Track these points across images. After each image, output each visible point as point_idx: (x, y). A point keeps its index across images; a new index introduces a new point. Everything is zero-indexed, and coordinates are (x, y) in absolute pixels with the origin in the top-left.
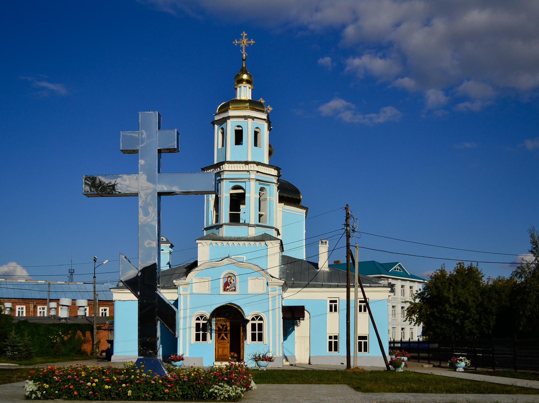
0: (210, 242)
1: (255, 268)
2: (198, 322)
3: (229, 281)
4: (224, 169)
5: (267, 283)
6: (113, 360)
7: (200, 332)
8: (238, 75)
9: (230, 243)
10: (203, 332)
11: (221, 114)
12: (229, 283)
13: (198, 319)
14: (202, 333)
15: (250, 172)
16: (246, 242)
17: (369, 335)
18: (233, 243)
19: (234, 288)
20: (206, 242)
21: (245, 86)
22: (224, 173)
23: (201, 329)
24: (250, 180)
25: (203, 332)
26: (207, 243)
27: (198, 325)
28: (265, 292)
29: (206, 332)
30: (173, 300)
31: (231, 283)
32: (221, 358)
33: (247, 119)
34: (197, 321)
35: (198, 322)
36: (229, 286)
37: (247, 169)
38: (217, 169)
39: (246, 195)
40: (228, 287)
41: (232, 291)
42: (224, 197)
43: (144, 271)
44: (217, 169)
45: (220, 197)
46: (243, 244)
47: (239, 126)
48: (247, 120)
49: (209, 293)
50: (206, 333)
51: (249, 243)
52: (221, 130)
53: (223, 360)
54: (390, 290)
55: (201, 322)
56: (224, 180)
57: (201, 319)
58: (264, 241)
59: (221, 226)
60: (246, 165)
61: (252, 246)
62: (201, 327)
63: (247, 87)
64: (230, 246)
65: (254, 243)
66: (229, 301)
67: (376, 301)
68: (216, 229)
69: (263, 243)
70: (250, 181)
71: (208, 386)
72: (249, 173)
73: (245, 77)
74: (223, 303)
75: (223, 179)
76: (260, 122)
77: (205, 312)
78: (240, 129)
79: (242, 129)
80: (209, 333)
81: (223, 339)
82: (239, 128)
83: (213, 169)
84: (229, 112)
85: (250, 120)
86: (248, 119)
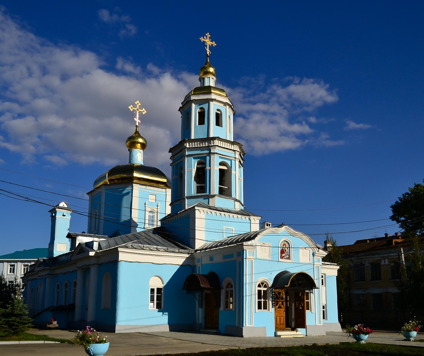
1: (304, 238)
2: (260, 289)
3: (284, 249)
4: (215, 144)
5: (313, 254)
6: (118, 330)
7: (261, 299)
8: (205, 68)
9: (223, 213)
10: (264, 300)
11: (200, 95)
12: (284, 251)
13: (259, 286)
14: (263, 301)
15: (236, 152)
17: (326, 305)
19: (288, 256)
20: (203, 209)
21: (213, 78)
22: (216, 147)
23: (262, 297)
25: (264, 300)
26: (200, 210)
27: (259, 292)
28: (312, 262)
29: (267, 300)
30: (178, 265)
31: (285, 250)
32: (279, 327)
34: (258, 288)
35: (260, 289)
36: (284, 254)
38: (204, 143)
40: (283, 255)
41: (286, 259)
43: (393, 220)
44: (204, 143)
45: (210, 170)
46: (228, 215)
47: (218, 110)
48: (225, 107)
49: (269, 259)
50: (267, 301)
51: (237, 216)
52: (199, 109)
53: (281, 329)
54: (339, 268)
55: (263, 289)
56: (216, 155)
57: (262, 286)
58: (249, 215)
59: (214, 196)
60: (232, 145)
61: (239, 219)
62: (262, 295)
65: (241, 217)
66: (285, 268)
67: (330, 277)
68: (204, 199)
69: (247, 218)
70: (235, 161)
71: (90, 350)
72: (235, 154)
73: (211, 70)
74: (283, 269)
75: (214, 153)
77: (266, 279)
78: (219, 112)
79: (220, 113)
80: (270, 301)
81: (280, 307)
82: (218, 111)
83: (198, 143)
84: (211, 95)
85: (228, 107)
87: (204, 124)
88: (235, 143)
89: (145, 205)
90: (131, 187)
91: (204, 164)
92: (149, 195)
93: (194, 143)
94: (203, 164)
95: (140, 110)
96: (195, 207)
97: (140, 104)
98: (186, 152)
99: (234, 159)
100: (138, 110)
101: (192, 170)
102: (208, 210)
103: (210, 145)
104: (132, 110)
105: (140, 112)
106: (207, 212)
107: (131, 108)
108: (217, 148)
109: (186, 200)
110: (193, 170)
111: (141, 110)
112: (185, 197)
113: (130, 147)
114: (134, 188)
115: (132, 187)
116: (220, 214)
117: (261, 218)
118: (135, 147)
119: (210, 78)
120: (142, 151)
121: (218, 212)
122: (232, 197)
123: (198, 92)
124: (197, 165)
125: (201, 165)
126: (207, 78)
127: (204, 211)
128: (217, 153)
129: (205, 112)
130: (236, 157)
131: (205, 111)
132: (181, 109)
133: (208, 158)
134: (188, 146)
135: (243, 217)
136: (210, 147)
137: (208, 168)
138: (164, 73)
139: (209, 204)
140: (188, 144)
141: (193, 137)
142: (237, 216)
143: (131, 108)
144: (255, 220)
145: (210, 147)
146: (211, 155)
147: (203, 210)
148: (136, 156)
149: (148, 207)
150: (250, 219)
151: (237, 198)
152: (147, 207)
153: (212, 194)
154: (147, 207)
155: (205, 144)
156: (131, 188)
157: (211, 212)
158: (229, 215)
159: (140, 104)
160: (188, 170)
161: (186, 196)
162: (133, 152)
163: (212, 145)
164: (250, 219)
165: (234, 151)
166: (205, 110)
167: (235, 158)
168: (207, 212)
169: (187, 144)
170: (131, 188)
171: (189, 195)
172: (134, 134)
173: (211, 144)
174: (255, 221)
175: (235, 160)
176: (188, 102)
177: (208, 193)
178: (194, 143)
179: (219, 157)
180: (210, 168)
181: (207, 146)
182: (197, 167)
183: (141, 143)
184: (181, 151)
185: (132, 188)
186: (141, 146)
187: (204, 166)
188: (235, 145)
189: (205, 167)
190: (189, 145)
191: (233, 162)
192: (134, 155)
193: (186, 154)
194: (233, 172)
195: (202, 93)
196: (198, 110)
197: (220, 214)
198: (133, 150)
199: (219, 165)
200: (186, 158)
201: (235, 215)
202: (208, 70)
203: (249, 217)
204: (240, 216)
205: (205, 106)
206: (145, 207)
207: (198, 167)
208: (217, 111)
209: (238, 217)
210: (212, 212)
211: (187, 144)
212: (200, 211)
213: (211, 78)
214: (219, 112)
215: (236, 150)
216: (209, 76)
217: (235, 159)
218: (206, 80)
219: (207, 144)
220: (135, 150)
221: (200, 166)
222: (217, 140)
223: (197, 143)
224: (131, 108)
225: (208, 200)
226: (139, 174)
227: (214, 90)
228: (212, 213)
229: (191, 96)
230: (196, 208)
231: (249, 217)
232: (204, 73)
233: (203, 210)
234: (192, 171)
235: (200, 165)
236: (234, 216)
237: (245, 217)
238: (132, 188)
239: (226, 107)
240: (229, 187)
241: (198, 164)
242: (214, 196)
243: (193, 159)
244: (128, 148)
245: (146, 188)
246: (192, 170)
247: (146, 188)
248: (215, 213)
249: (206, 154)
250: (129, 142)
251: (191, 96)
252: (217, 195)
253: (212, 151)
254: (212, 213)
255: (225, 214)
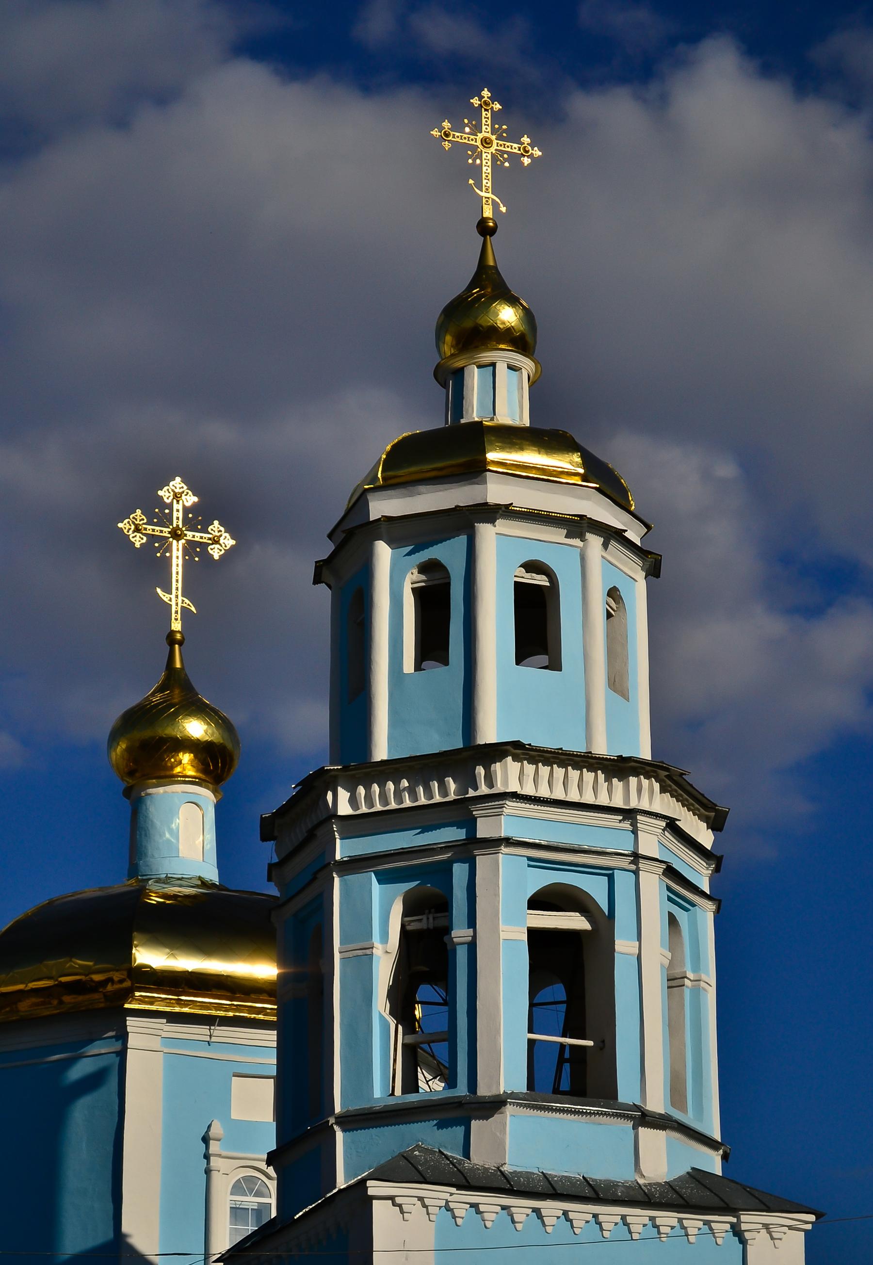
0: (447, 1196)
4: (499, 788)
9: (552, 1208)
11: (422, 488)
16: (638, 1211)
18: (595, 1216)
21: (517, 364)
24: (643, 865)
26: (398, 1200)
33: (583, 539)
37: (618, 802)
38: (435, 785)
39: (617, 947)
42: (501, 941)
44: (435, 785)
45: (472, 947)
47: (532, 566)
48: (577, 542)
51: (652, 1219)
52: (415, 571)
56: (504, 849)
59: (495, 1105)
60: (615, 780)
63: (523, 370)
64: (519, 1227)
65: (674, 1222)
68: (441, 1126)
69: (722, 1223)
70: (636, 873)
72: (635, 832)
75: (495, 843)
76: (619, 560)
78: (541, 580)
79: (548, 584)
83: (405, 783)
84: (486, 483)
85: (595, 541)
86: (588, 536)
87: (444, 660)
88: (633, 764)
89: (207, 1148)
90: (116, 1038)
91: (443, 905)
92: (233, 1078)
93: (382, 786)
94: (436, 912)
95: (190, 535)
96: (369, 1183)
97: (190, 499)
98: (338, 841)
99: (625, 863)
100: (176, 535)
101: (368, 952)
102: (451, 1194)
103: (471, 793)
104: (138, 541)
105: (191, 548)
106: (448, 1209)
107: (137, 530)
108: (512, 805)
109: (340, 1135)
110: (378, 950)
111: (198, 536)
112: (332, 1120)
113: (131, 773)
114: (132, 1041)
115: (123, 1036)
116: (537, 1211)
117: (812, 1218)
118: (163, 774)
119: (493, 365)
120: (207, 796)
121: (522, 1206)
122: (616, 1098)
123: (413, 469)
124: (405, 914)
125: (424, 917)
126: (479, 367)
127: (427, 1201)
128: (508, 842)
129: (448, 585)
130: (642, 851)
131: (449, 584)
132: (326, 573)
133: (459, 871)
134: (344, 809)
135: (694, 1223)
136: (472, 808)
137: (460, 933)
138: (694, 38)
139: (469, 1158)
140: (348, 795)
141: (381, 752)
142: (646, 1220)
143: (137, 526)
144: (775, 1235)
145: (472, 808)
146: (476, 852)
147: (421, 1199)
148: (171, 831)
149: (224, 1153)
150: (737, 1229)
151: (657, 1103)
152: (219, 1156)
153: (484, 1090)
154: (219, 1156)
155: (444, 791)
156: (118, 1046)
157: (472, 1205)
158: (595, 1216)
159: (190, 499)
160: (350, 954)
161: (338, 1109)
162: (148, 803)
163: (484, 790)
164: (737, 1232)
165: (629, 814)
166: (449, 577)
167: (636, 857)
168: (448, 1209)
169: (343, 795)
170: (118, 1046)
171: (356, 1106)
172: (153, 694)
173: (476, 788)
174: (772, 1238)
175: (633, 867)
176: (350, 534)
177: (462, 1090)
178: (382, 786)
179: (530, 859)
180: (474, 937)
181: (452, 797)
182: (403, 926)
183: (198, 748)
184: (311, 836)
185: (120, 1042)
186: (201, 767)
187: (441, 922)
188: (633, 780)
189: (448, 930)
190: (353, 801)
191: (623, 881)
192: (157, 823)
193: (338, 857)
194: (624, 945)
195: (433, 474)
196: (412, 578)
197: (537, 1211)
198: (150, 791)
199: (530, 907)
200: (337, 881)
201: (639, 1217)
202: (485, 321)
203: (734, 1220)
204: (667, 1219)
205: (442, 552)
206: (207, 1157)
207: (409, 928)
208: (528, 575)
209: (658, 1221)
210: (482, 1208)
211: (343, 795)
212: (400, 1206)
213: (502, 368)
214: (539, 577)
215: (645, 805)
216: (487, 356)
217: (631, 863)
218: (475, 378)
219: (452, 786)
220: (161, 790)
221: (420, 920)
222: (509, 759)
223: (397, 783)
224: (137, 530)
225: (463, 1127)
226: (167, 950)
227: (502, 449)
228: (478, 1212)
229: (370, 497)
230: (375, 1188)
231: (734, 1220)
232: (458, 343)
233: (421, 1199)
234: (372, 954)
235: (422, 914)
236: (629, 1220)
237: (707, 1223)
238: (120, 1042)
239: (581, 544)
240: (603, 1042)
241: (411, 908)
242: (495, 1105)
243: (380, 882)
244: (123, 780)
245: (213, 1039)
246: (368, 952)
247: (213, 1039)
248: (504, 1208)
249: (449, 847)
250: (122, 746)
251: (370, 497)
252: (513, 1095)
253: (484, 830)
254: (478, 1212)
255: (624, 1217)
